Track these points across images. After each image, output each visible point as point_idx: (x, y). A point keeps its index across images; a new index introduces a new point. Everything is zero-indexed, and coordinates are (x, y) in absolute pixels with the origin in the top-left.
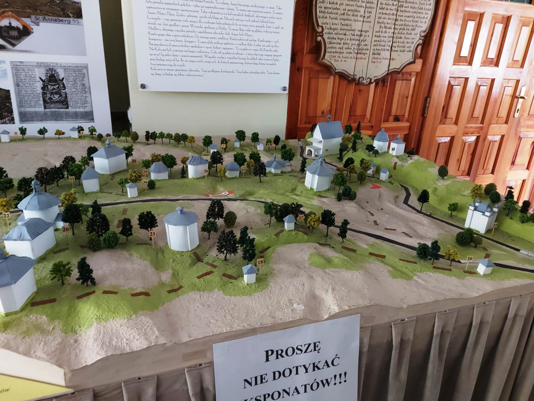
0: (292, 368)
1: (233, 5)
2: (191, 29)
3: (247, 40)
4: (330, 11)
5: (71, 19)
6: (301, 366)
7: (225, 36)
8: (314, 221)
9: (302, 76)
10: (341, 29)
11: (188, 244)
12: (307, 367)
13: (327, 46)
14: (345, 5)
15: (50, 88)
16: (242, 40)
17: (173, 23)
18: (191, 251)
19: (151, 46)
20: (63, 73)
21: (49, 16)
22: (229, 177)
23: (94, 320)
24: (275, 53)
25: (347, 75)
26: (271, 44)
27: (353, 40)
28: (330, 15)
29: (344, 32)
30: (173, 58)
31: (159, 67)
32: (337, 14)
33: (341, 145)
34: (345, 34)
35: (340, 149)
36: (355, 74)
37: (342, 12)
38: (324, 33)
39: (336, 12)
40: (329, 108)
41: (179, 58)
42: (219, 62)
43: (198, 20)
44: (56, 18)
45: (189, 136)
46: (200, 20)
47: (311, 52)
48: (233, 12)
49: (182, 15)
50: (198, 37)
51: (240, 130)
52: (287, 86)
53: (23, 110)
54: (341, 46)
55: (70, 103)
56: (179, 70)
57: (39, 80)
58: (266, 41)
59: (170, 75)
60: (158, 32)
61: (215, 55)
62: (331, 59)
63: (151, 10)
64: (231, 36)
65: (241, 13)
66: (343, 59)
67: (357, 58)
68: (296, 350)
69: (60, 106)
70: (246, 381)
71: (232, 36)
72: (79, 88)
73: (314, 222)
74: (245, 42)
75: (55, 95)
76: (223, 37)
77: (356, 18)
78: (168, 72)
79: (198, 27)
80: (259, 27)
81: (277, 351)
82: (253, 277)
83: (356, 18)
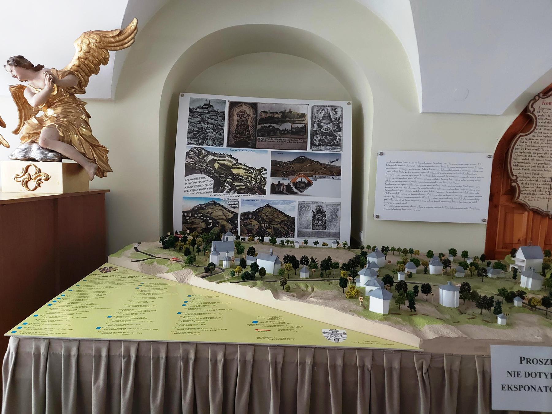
0: (536, 373)
1: (446, 164)
2: (414, 180)
3: (455, 186)
4: (522, 164)
5: (334, 176)
6: (542, 373)
7: (438, 184)
8: (537, 302)
9: (499, 211)
10: (533, 177)
11: (454, 304)
12: (547, 375)
13: (521, 189)
14: (535, 160)
15: (318, 217)
16: (451, 186)
17: (402, 177)
18: (456, 308)
19: (386, 192)
20: (326, 208)
21: (322, 175)
22: (457, 277)
23: (425, 324)
24: (477, 195)
25: (541, 211)
26: (473, 188)
27: (545, 184)
28: (523, 167)
29: (536, 179)
30: (400, 199)
31: (390, 205)
32: (529, 166)
33: (543, 264)
34: (537, 181)
35: (542, 267)
36: (549, 210)
37: (534, 165)
38: (518, 180)
39: (528, 165)
40: (525, 237)
41: (404, 199)
42: (432, 201)
43: (419, 174)
44: (326, 176)
45: (414, 250)
46: (421, 175)
47: (506, 193)
48: (445, 169)
49: (408, 172)
50: (418, 185)
51: (452, 248)
52: (486, 218)
53: (300, 229)
54: (534, 189)
55: (327, 227)
56: (403, 207)
57: (312, 212)
58: (470, 187)
59: (396, 209)
60: (391, 183)
61: (430, 197)
62: (525, 199)
63: (388, 170)
64: (442, 184)
65: (451, 169)
66: (536, 199)
67: (549, 198)
68: (539, 362)
69: (321, 228)
70: (508, 372)
71: (444, 184)
72: (334, 217)
73: (537, 302)
74: (452, 188)
75: (319, 221)
76: (436, 184)
77: (546, 169)
78: (395, 208)
79: (419, 179)
80: (464, 177)
81: (527, 359)
82: (505, 321)
83: (546, 169)
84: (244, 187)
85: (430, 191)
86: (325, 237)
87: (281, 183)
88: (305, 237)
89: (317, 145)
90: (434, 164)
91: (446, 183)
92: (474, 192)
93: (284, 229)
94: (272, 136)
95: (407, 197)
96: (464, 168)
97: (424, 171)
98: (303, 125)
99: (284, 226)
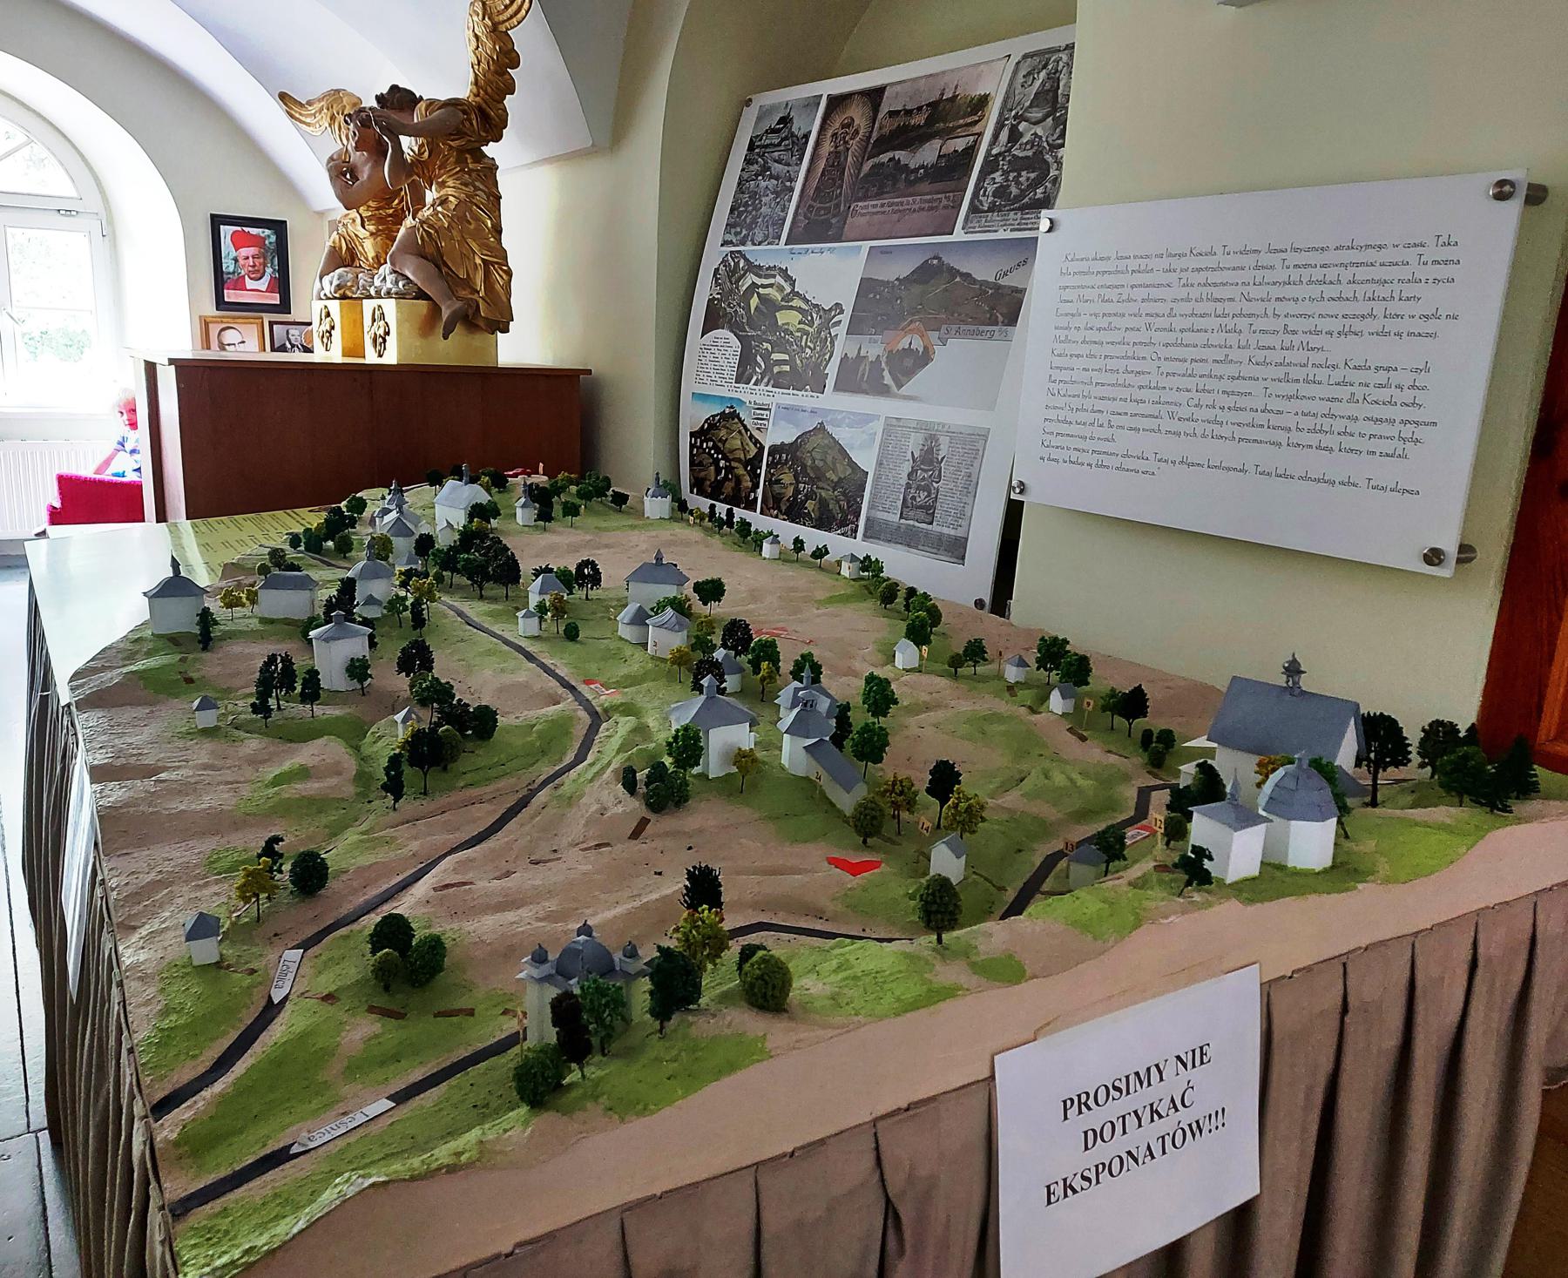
7: (1235, 354)
17: (1104, 322)
42: (1204, 436)
48: (1270, 276)
49: (1129, 300)
74: (1296, 373)
76: (1227, 356)
84: (787, 368)
85: (1201, 387)
86: (928, 549)
87: (863, 353)
88: (879, 539)
89: (986, 212)
90: (1425, 264)
91: (1269, 348)
92: (1400, 397)
93: (840, 507)
94: (887, 193)
95: (1113, 413)
96: (1358, 265)
97: (1183, 293)
98: (972, 138)
99: (842, 498)
